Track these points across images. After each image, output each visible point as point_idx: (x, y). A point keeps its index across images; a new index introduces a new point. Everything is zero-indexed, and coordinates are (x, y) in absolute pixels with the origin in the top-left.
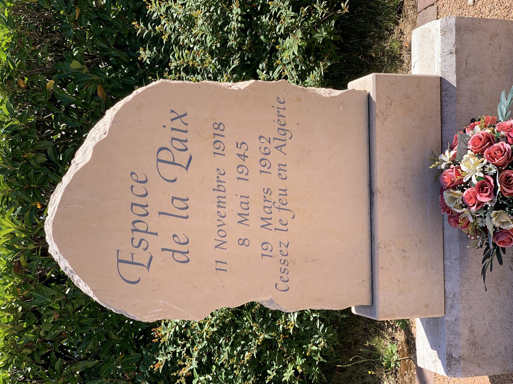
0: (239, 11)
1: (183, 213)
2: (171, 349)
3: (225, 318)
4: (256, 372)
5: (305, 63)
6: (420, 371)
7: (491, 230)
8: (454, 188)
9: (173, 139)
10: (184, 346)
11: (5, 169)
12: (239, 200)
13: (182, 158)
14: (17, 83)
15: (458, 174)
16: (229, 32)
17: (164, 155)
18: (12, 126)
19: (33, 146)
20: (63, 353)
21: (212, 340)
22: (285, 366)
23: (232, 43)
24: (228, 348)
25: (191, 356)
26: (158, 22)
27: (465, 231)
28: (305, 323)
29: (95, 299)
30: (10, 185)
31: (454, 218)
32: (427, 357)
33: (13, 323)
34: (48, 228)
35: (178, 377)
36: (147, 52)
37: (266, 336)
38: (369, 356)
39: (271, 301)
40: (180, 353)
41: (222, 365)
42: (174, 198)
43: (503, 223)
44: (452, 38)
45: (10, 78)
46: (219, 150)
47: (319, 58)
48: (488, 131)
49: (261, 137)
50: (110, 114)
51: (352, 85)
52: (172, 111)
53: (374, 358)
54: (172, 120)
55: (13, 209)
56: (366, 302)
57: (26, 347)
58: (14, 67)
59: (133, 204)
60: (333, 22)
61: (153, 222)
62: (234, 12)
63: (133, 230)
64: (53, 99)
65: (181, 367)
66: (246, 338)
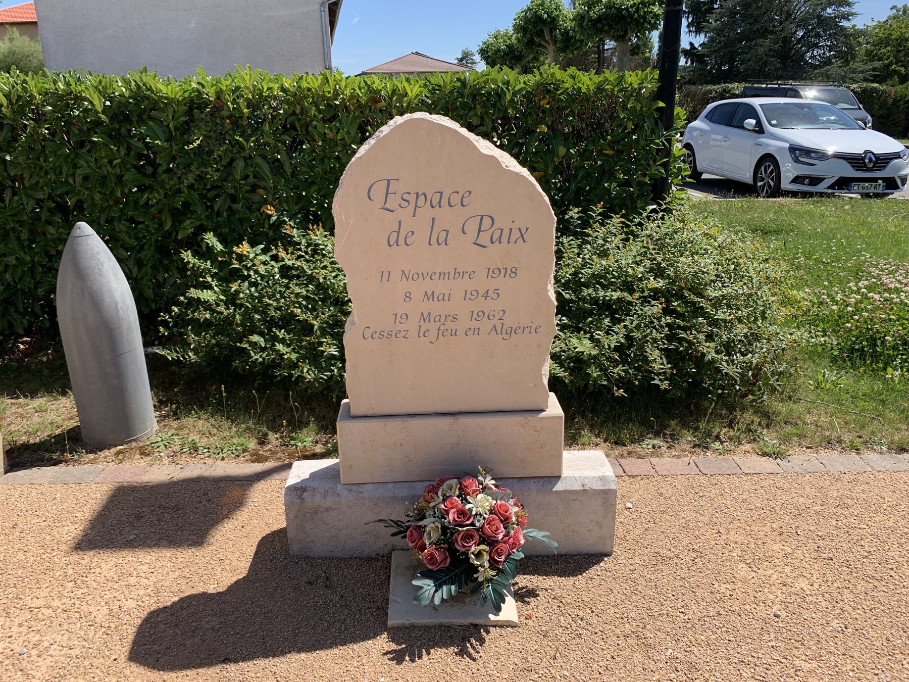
0: (615, 297)
1: (434, 241)
2: (304, 241)
3: (332, 290)
4: (282, 318)
5: (568, 358)
6: (289, 466)
7: (421, 523)
8: (460, 489)
9: (502, 230)
10: (306, 253)
11: (465, 87)
12: (447, 293)
13: (484, 239)
14: (544, 98)
15: (474, 491)
16: (596, 290)
17: (487, 222)
18: (505, 93)
19: (487, 112)
20: (295, 145)
21: (311, 279)
22: (288, 346)
23: (586, 292)
24: (305, 293)
25: (297, 259)
26: (603, 225)
27: (421, 499)
28: (328, 362)
29: (353, 159)
30: (451, 92)
31: (434, 490)
32: (301, 470)
33: (323, 96)
34: (418, 115)
35: (276, 247)
36: (576, 216)
37: (316, 327)
38: (300, 422)
39: (353, 324)
40: (300, 250)
41: (289, 288)
42: (448, 231)
43: (429, 534)
44: (597, 486)
45: (549, 91)
46: (492, 273)
47: (572, 371)
48: (514, 519)
49: (504, 312)
50: (525, 172)
51: (552, 395)
52: (527, 229)
53: (297, 425)
54: (520, 229)
55: (428, 95)
56: (353, 412)
57: (302, 109)
58: (560, 95)
59: (441, 193)
60: (605, 383)
61: (426, 212)
62: (613, 293)
63: (417, 193)
64: (530, 132)
65: (286, 250)
66: (314, 309)
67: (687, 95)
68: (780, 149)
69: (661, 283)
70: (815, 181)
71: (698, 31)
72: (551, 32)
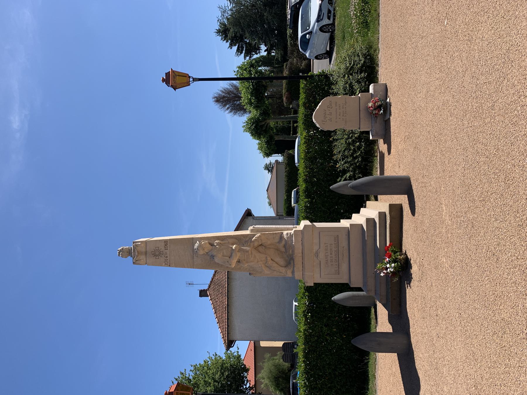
68: (318, 26)
69: (347, 76)
70: (329, 12)
71: (259, 49)
72: (261, 122)
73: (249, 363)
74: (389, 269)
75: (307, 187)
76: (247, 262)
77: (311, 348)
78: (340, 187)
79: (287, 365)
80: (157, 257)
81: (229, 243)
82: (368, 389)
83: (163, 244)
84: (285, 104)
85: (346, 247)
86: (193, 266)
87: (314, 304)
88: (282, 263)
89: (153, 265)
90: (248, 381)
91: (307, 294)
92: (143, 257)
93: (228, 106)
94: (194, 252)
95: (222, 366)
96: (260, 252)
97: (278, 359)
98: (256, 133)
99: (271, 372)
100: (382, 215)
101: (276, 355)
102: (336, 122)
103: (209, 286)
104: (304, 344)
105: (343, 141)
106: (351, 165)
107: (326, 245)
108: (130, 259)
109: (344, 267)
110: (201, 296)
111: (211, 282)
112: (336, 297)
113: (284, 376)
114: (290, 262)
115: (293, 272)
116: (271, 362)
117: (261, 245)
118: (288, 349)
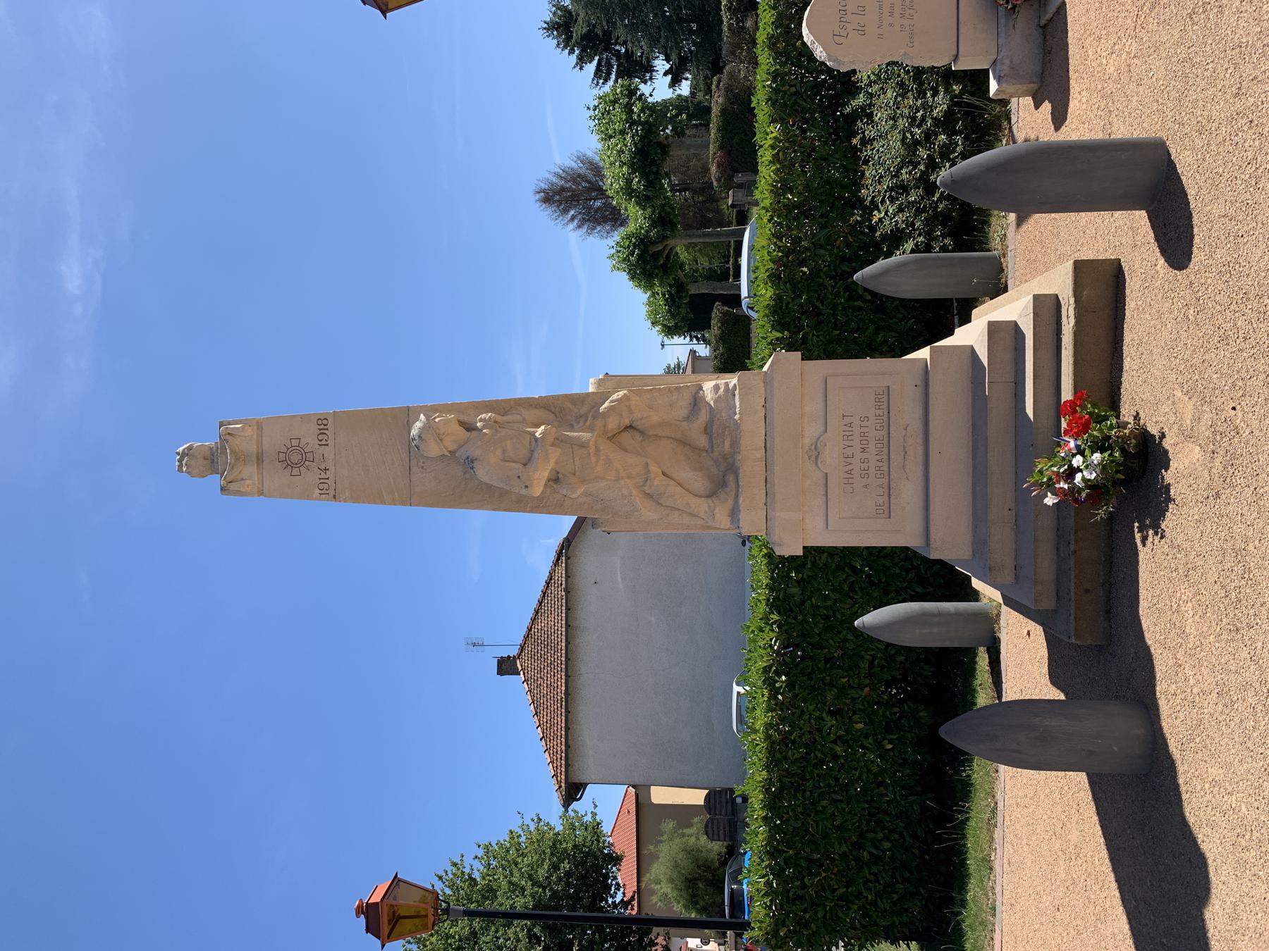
61: (849, 17)
67: (733, 53)
71: (650, 69)
72: (653, 243)
73: (623, 841)
74: (1078, 477)
75: (778, 298)
76: (583, 481)
77: (786, 780)
78: (885, 272)
79: (716, 847)
80: (295, 471)
81: (524, 421)
82: (963, 903)
83: (314, 429)
84: (715, 183)
85: (917, 426)
86: (409, 498)
87: (797, 647)
88: (699, 483)
89: (282, 495)
90: (618, 887)
91: (775, 617)
92: (250, 470)
93: (572, 212)
94: (413, 449)
95: (555, 848)
96: (625, 450)
97: (696, 837)
98: (644, 273)
99: (676, 865)
100: (1047, 308)
101: (690, 825)
102: (880, 37)
103: (522, 648)
104: (767, 767)
105: (895, 142)
106: (919, 212)
107: (847, 420)
108: (215, 481)
109: (909, 494)
110: (501, 672)
111: (526, 637)
112: (868, 620)
113: (710, 876)
114: (724, 479)
115: (734, 514)
116: (678, 841)
117: (630, 427)
118: (723, 810)
